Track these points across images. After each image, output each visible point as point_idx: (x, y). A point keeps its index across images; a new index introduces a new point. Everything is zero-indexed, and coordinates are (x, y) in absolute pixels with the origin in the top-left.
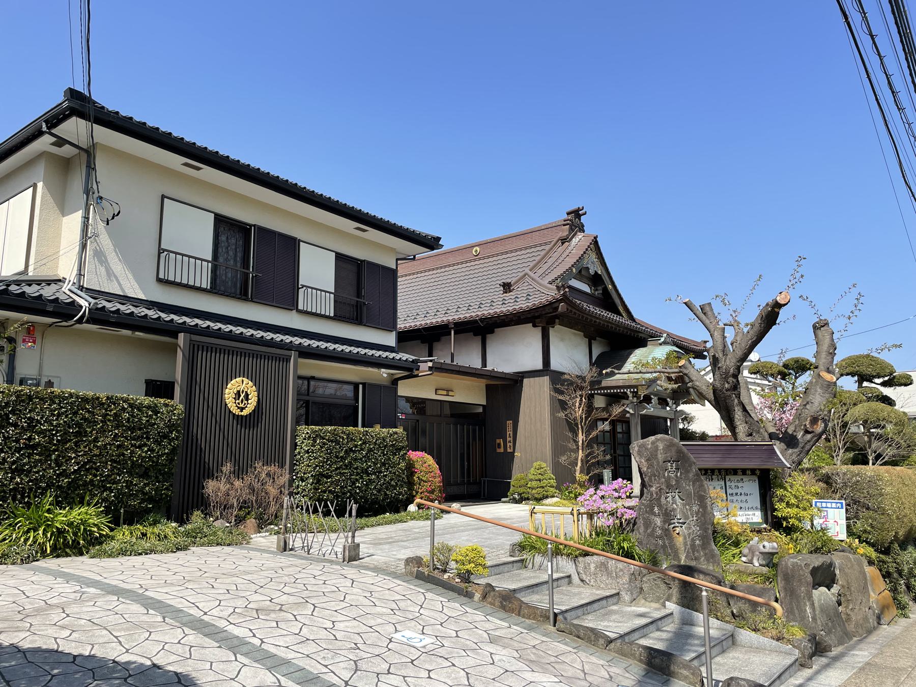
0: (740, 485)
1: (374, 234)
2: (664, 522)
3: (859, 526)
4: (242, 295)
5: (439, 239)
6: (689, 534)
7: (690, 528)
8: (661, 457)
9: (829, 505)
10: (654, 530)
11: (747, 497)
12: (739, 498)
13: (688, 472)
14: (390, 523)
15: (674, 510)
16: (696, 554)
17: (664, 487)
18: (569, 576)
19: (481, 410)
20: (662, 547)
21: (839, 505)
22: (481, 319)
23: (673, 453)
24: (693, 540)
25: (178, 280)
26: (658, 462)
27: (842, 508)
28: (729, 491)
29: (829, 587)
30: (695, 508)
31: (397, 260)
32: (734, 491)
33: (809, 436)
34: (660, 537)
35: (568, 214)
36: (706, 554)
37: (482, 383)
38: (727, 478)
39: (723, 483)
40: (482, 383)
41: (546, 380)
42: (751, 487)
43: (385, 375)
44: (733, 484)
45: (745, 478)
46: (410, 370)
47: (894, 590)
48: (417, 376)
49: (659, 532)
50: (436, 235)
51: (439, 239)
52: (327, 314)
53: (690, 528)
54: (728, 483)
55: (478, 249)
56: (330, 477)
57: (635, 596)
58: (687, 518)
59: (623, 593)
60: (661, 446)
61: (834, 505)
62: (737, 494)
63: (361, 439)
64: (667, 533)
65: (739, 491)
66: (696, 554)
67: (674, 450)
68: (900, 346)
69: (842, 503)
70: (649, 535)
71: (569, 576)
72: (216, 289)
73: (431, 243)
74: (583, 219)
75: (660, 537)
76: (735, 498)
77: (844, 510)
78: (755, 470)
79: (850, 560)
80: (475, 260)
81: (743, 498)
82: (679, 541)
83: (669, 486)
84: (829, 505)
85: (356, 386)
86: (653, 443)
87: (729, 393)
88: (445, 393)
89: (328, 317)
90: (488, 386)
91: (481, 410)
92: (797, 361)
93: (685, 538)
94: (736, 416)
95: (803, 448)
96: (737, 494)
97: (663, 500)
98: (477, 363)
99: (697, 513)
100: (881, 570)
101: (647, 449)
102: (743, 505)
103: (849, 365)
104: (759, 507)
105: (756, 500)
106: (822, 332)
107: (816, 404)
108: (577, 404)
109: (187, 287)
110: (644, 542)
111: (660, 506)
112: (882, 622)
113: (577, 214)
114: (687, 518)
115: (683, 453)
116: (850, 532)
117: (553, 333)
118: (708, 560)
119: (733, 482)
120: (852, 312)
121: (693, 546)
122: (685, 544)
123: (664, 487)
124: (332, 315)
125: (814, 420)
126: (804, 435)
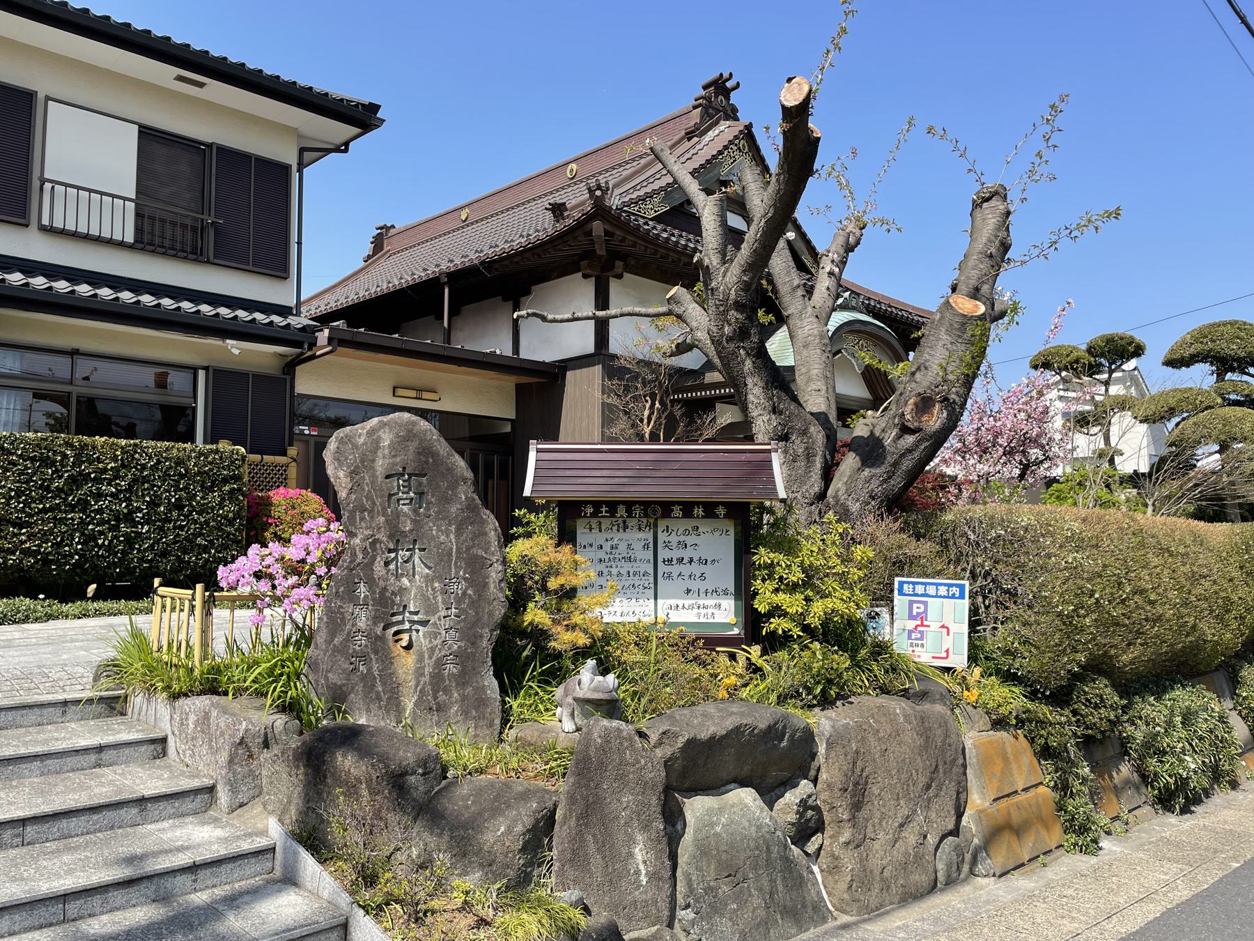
0: (690, 540)
1: (217, 91)
2: (375, 619)
3: (996, 640)
4: (194, 254)
5: (374, 108)
6: (432, 650)
7: (436, 635)
8: (381, 465)
9: (931, 590)
10: (350, 638)
11: (703, 568)
12: (686, 569)
13: (445, 500)
14: (99, 613)
15: (402, 591)
16: (442, 697)
17: (382, 536)
18: (164, 740)
19: (508, 428)
20: (364, 678)
21: (955, 590)
22: (483, 263)
23: (409, 456)
24: (440, 664)
25: (106, 234)
26: (374, 476)
27: (962, 597)
28: (663, 554)
29: (770, 794)
30: (458, 588)
31: (302, 151)
32: (675, 554)
33: (910, 440)
34: (364, 657)
35: (705, 88)
36: (464, 698)
37: (509, 383)
38: (662, 524)
39: (649, 536)
40: (509, 383)
41: (598, 369)
42: (717, 543)
43: (236, 352)
44: (674, 539)
45: (705, 526)
46: (297, 344)
47: (1063, 788)
48: (313, 357)
49: (361, 640)
50: (366, 99)
51: (374, 108)
52: (118, 236)
53: (436, 635)
54: (662, 537)
55: (574, 166)
56: (28, 525)
57: (242, 798)
58: (431, 610)
59: (219, 787)
60: (386, 438)
61: (943, 591)
62: (680, 560)
63: (115, 459)
64: (378, 645)
65: (687, 554)
66: (442, 697)
67: (413, 446)
68: (1117, 214)
69: (962, 587)
70: (336, 650)
71: (164, 740)
72: (148, 240)
73: (363, 117)
74: (735, 98)
75: (364, 657)
76: (675, 569)
77: (966, 603)
78: (715, 505)
79: (892, 719)
80: (569, 186)
81: (696, 569)
82: (406, 665)
83: (397, 538)
84: (931, 590)
85: (194, 370)
86: (372, 432)
87: (732, 346)
88: (413, 394)
89: (121, 245)
90: (519, 387)
91: (508, 428)
92: (1110, 340)
93: (421, 658)
94: (751, 397)
95: (895, 465)
96: (680, 560)
97: (379, 568)
98: (501, 346)
99: (459, 601)
100: (1032, 741)
101: (355, 446)
102: (694, 585)
103: (1197, 340)
104: (732, 589)
105: (728, 580)
106: (990, 215)
107: (935, 369)
108: (646, 413)
109: (98, 240)
110: (323, 667)
111: (371, 582)
112: (980, 868)
113: (720, 87)
114: (431, 610)
115: (434, 455)
116: (973, 659)
117: (615, 288)
118: (466, 713)
119: (673, 533)
120: (1039, 155)
121: (437, 678)
122: (419, 672)
123: (382, 536)
124: (130, 238)
125: (924, 404)
126: (899, 437)
